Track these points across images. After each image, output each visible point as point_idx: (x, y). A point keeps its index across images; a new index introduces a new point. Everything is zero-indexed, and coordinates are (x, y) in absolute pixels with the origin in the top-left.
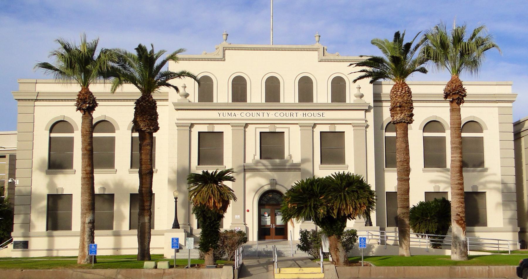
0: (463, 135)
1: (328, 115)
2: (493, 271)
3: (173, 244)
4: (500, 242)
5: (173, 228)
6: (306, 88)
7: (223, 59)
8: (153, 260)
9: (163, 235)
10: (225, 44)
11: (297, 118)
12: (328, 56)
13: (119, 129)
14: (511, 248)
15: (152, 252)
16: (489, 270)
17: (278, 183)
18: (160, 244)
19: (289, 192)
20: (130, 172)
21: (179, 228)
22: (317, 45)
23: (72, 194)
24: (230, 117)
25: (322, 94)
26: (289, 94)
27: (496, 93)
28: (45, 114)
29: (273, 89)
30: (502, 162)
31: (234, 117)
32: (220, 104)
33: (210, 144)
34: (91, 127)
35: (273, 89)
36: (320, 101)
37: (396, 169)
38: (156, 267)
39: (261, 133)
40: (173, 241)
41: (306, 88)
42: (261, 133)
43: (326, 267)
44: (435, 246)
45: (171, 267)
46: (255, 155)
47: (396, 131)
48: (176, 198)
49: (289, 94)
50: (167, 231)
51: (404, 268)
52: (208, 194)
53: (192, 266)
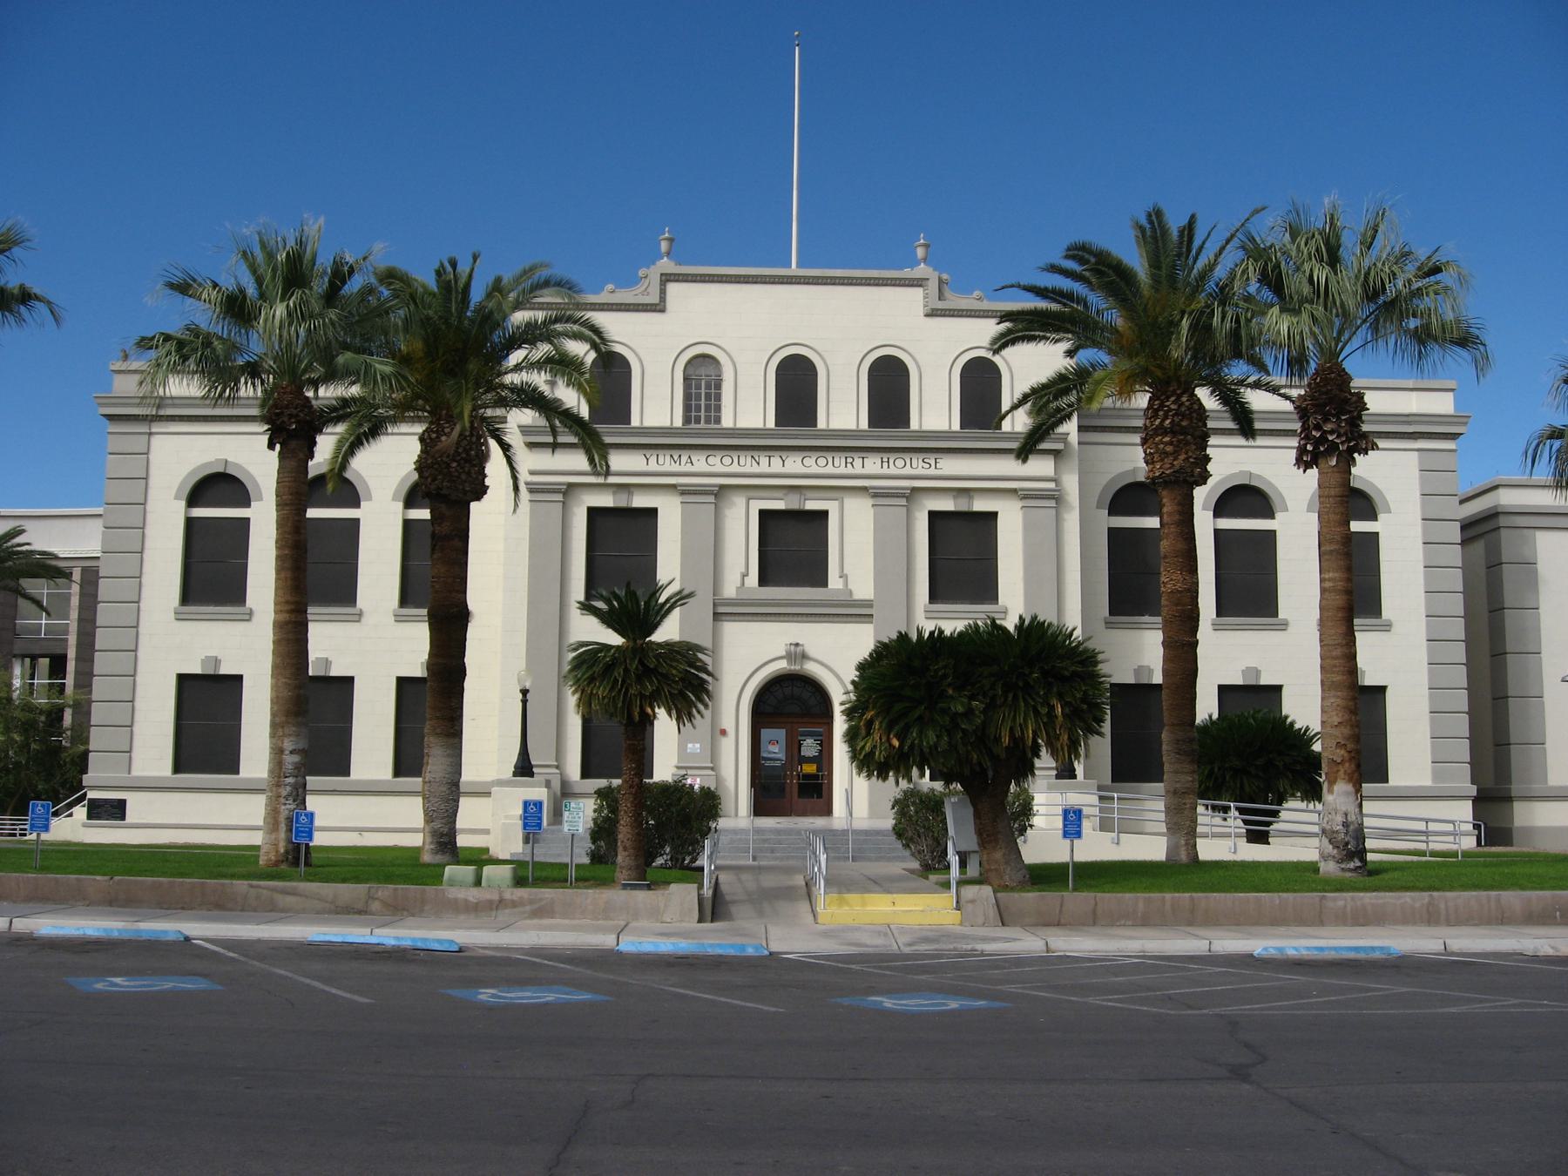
0: (312, 513)
1: (951, 465)
2: (1442, 906)
3: (1065, 826)
4: (1433, 827)
5: (515, 774)
6: (889, 385)
7: (659, 307)
8: (468, 863)
9: (488, 794)
10: (666, 265)
11: (864, 471)
12: (955, 301)
13: (369, 498)
15: (462, 841)
16: (1430, 904)
17: (811, 652)
18: (491, 822)
20: (399, 619)
21: (531, 775)
22: (922, 270)
23: (352, 678)
25: (935, 405)
26: (843, 405)
27: (1414, 410)
28: (179, 455)
29: (796, 384)
30: (1428, 605)
34: (300, 489)
35: (796, 384)
36: (649, 422)
37: (1159, 619)
38: (478, 882)
39: (762, 513)
40: (525, 810)
41: (889, 385)
42: (762, 513)
43: (970, 892)
44: (1258, 836)
45: (519, 881)
46: (745, 575)
47: (1159, 513)
48: (525, 692)
49: (843, 405)
50: (501, 783)
51: (1192, 899)
52: (636, 678)
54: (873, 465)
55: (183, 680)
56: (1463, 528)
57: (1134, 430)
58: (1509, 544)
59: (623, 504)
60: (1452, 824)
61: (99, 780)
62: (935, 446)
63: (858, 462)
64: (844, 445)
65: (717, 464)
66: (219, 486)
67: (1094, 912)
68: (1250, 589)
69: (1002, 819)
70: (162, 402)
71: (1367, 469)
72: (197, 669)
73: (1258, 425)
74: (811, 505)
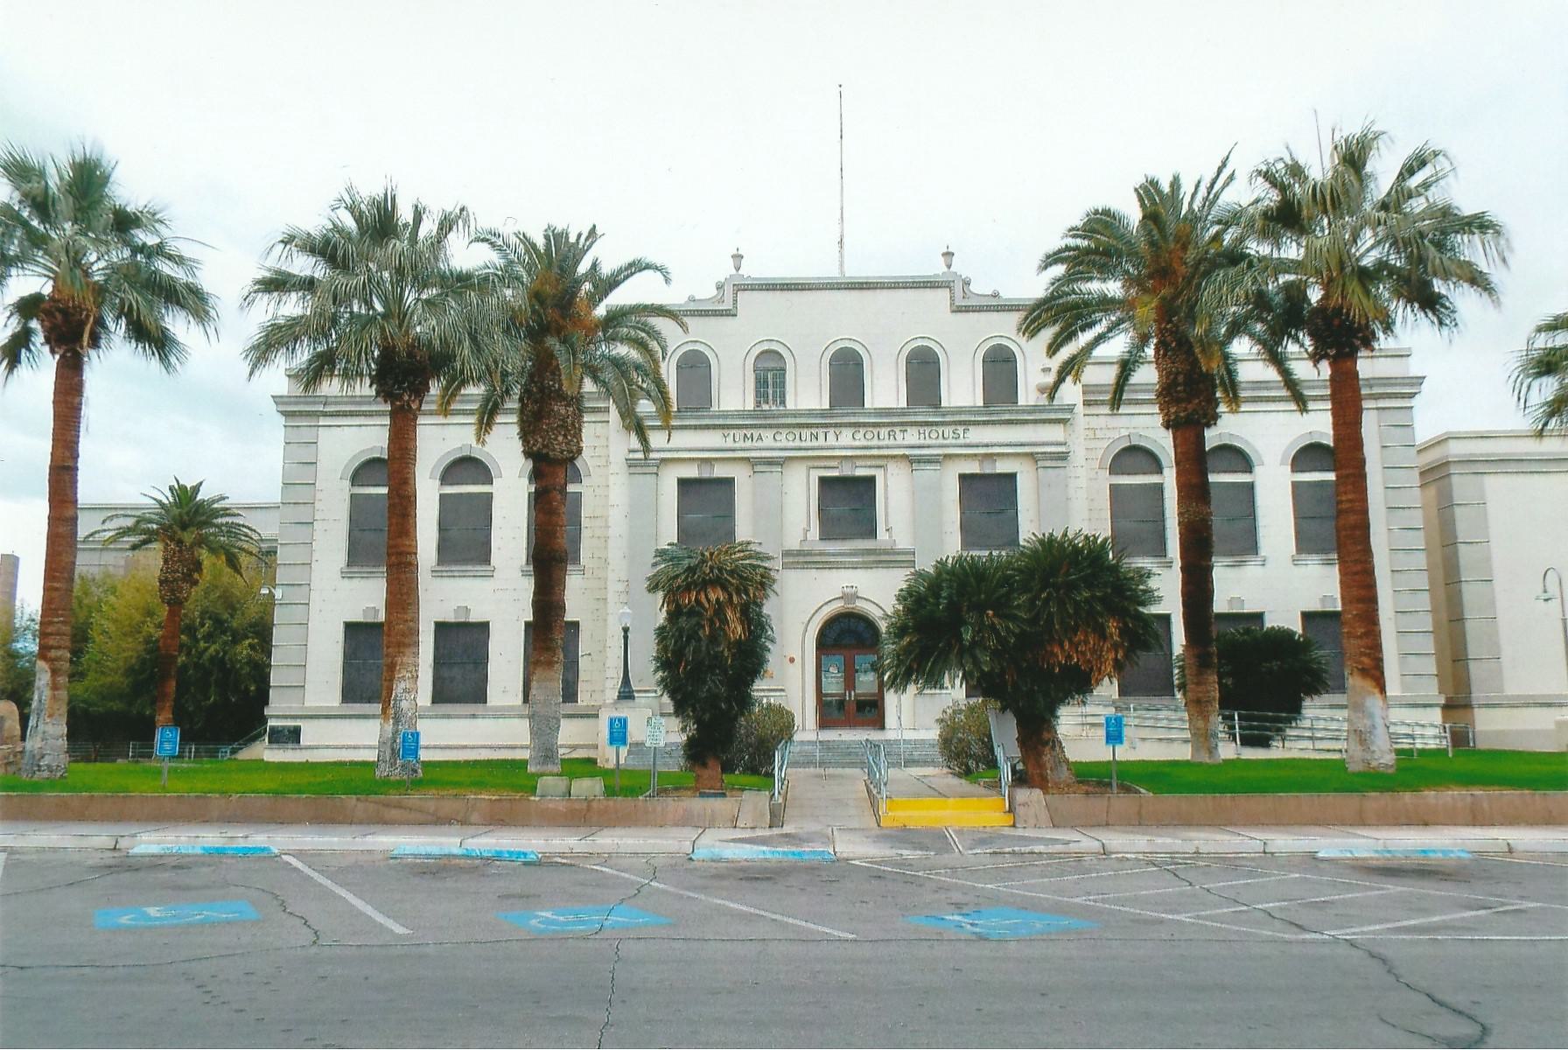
1: (977, 435)
2: (1485, 805)
6: (923, 370)
14: (1432, 744)
19: (1049, 544)
20: (345, 575)
24: (748, 444)
25: (962, 386)
26: (885, 388)
29: (847, 373)
31: (760, 444)
32: (725, 415)
33: (706, 497)
35: (847, 373)
41: (923, 370)
43: (1023, 794)
45: (610, 792)
48: (626, 630)
49: (885, 388)
53: (662, 792)
54: (912, 436)
55: (351, 628)
56: (1422, 474)
57: (1103, 403)
58: (1461, 486)
59: (706, 475)
60: (1427, 729)
61: (278, 709)
62: (965, 419)
63: (831, 436)
64: (890, 419)
65: (784, 439)
66: (1134, 456)
67: (1139, 813)
68: (467, 542)
69: (1036, 733)
70: (316, 400)
71: (1228, 427)
72: (451, 618)
73: (1243, 394)
74: (860, 472)
